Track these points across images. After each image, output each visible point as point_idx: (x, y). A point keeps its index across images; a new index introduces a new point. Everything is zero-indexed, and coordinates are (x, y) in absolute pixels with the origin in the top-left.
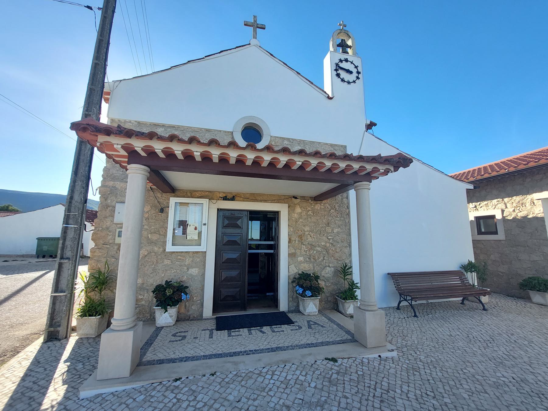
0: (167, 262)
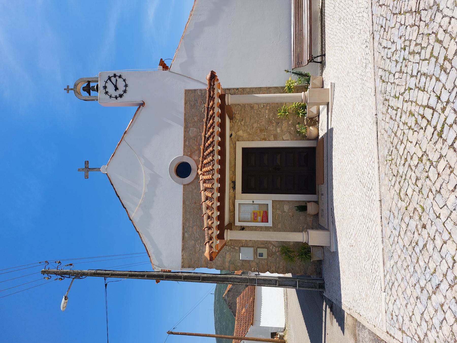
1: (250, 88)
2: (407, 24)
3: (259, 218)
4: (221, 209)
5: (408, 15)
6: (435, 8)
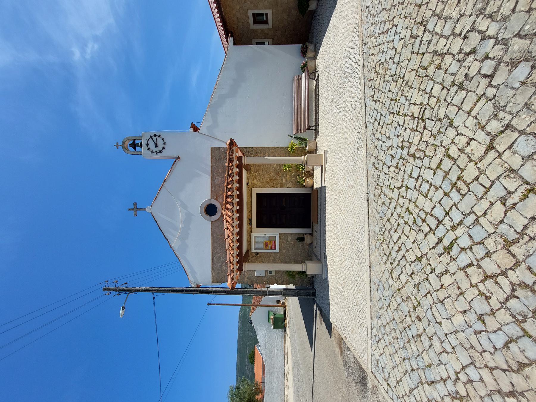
0: (284, 251)
1: (262, 148)
2: (406, 126)
3: (270, 246)
4: (240, 241)
5: (407, 118)
6: (446, 122)
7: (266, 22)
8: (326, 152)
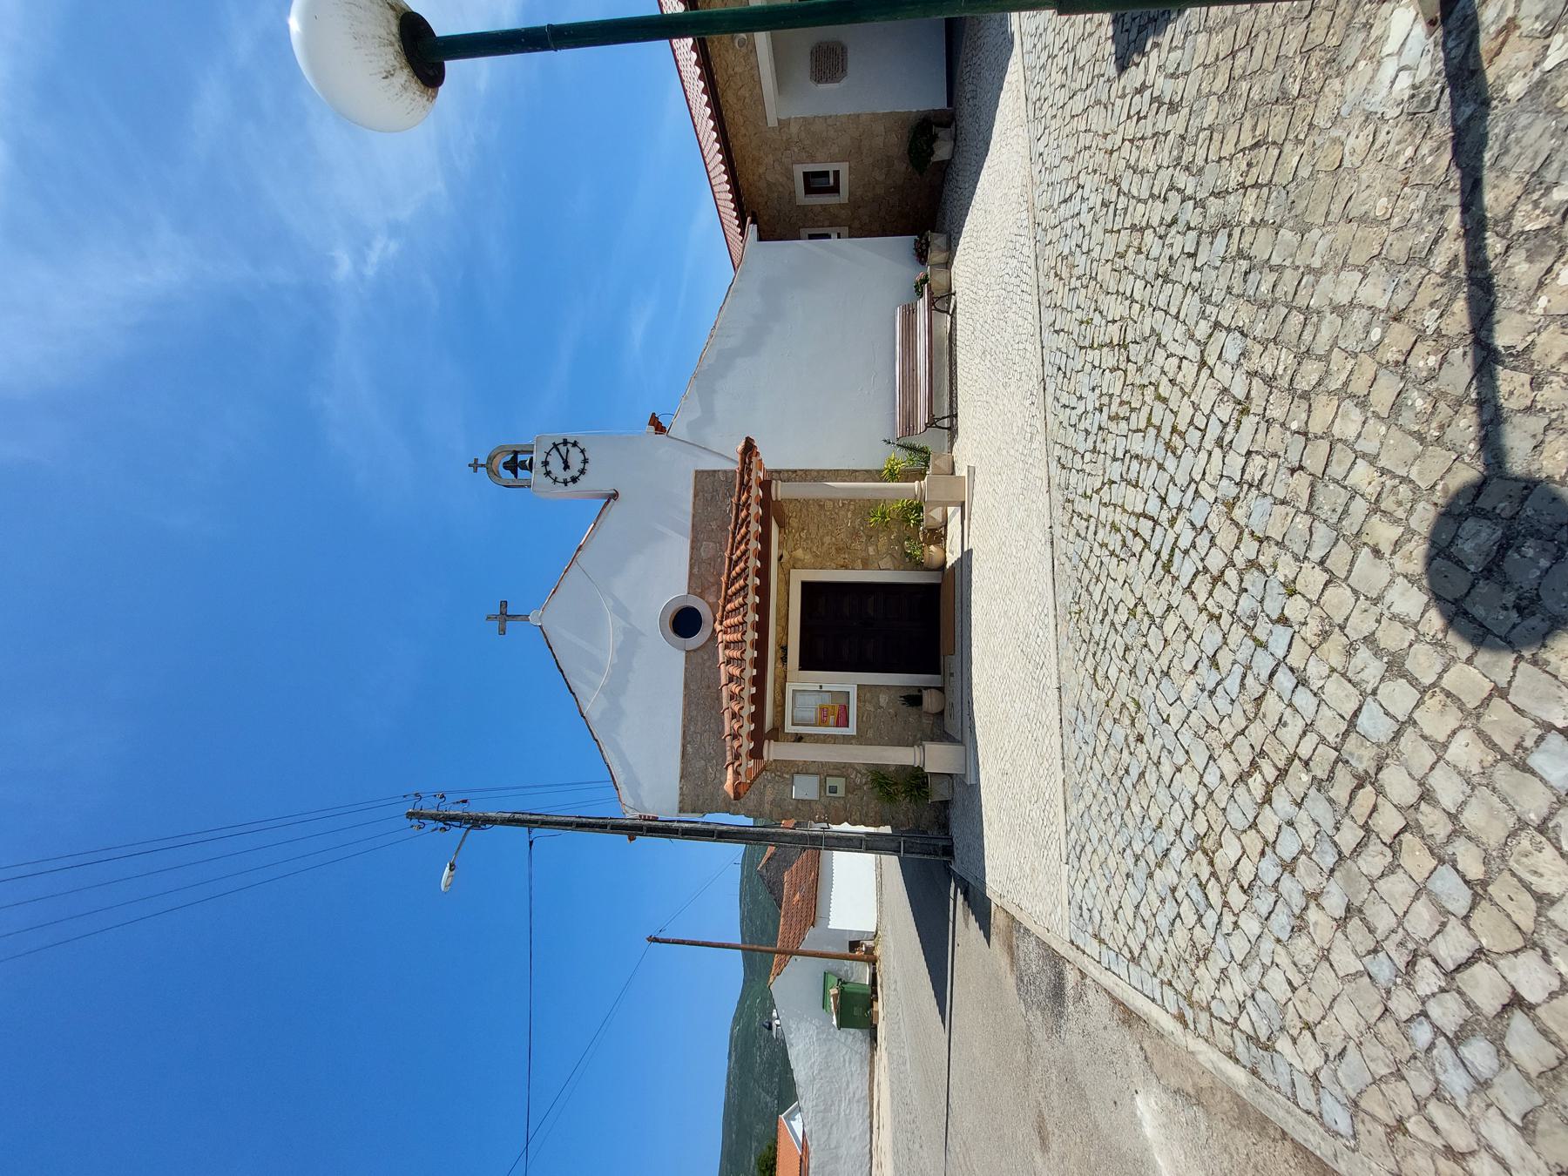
3: (832, 719)
5: (1105, 349)
7: (835, 190)
8: (971, 471)
